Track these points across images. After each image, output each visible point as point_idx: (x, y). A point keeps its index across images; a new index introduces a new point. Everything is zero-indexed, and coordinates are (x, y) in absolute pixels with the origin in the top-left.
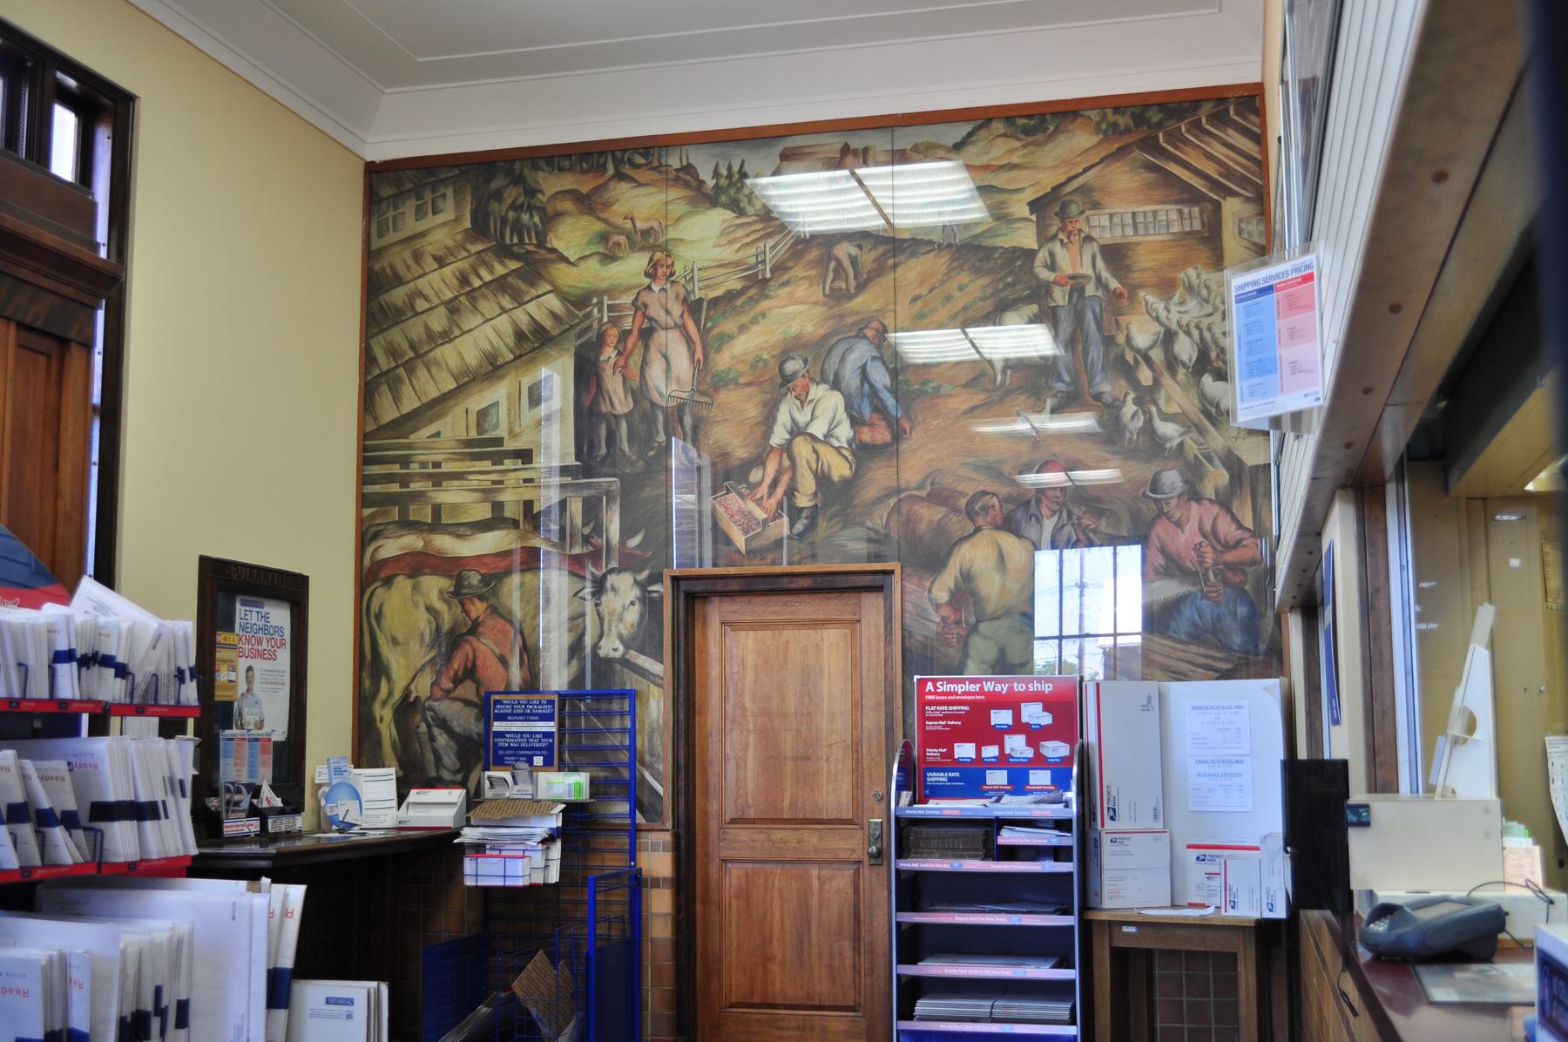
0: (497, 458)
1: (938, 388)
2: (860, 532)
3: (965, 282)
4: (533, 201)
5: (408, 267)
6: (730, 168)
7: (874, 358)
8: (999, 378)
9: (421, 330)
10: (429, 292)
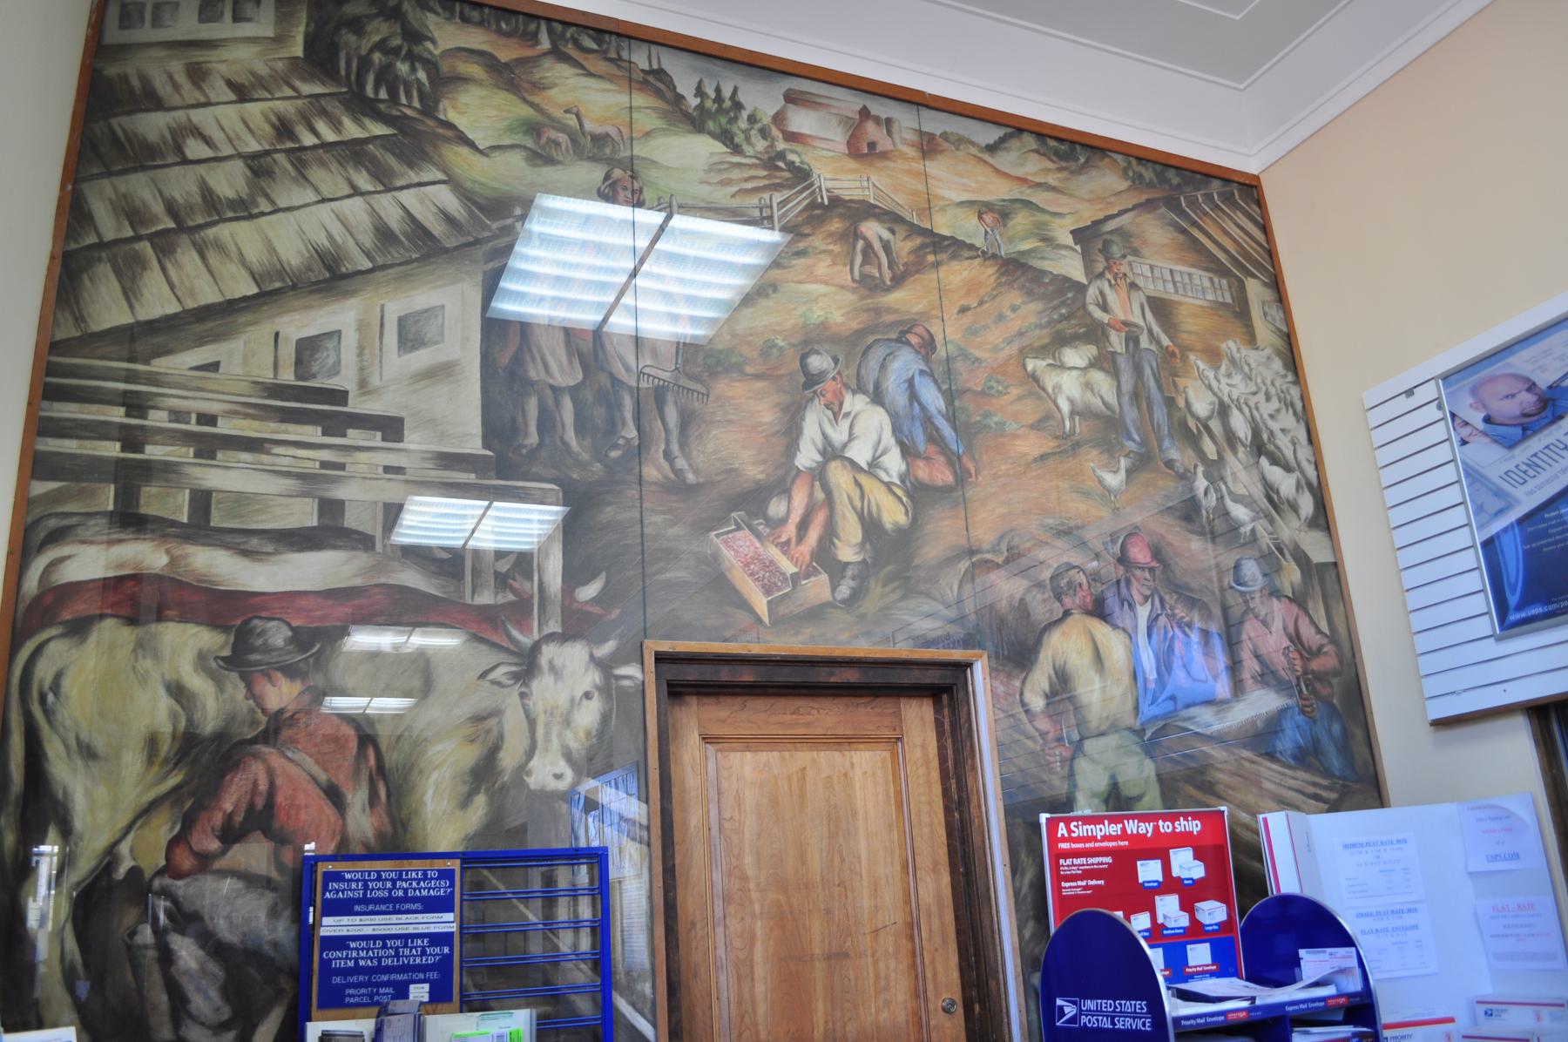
0: (336, 424)
1: (1001, 424)
2: (927, 606)
3: (1018, 301)
4: (417, 50)
5: (176, 87)
6: (718, 90)
7: (922, 372)
8: (1068, 424)
9: (194, 189)
10: (217, 135)
